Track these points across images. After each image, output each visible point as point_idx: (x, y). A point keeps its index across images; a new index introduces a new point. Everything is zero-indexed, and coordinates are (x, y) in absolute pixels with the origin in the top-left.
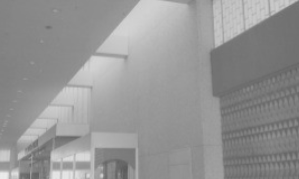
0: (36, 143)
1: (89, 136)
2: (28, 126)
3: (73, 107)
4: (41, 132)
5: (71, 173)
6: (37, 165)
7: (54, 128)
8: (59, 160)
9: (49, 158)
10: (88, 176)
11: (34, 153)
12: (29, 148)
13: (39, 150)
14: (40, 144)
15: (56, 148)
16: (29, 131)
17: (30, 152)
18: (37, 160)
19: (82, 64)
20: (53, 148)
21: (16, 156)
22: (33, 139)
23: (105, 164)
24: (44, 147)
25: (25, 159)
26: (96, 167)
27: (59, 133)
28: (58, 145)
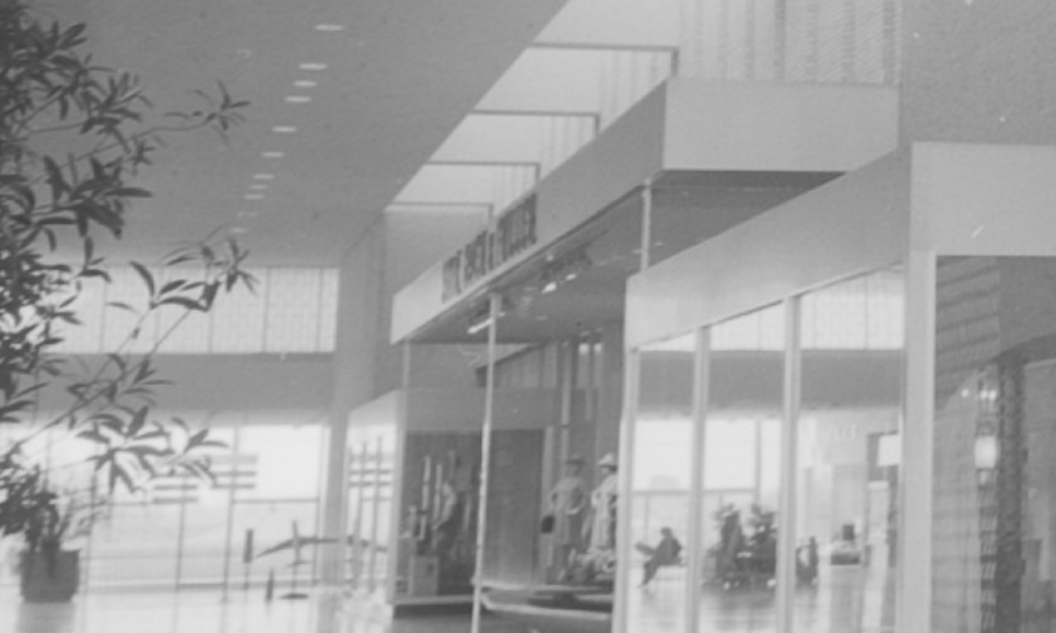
0: (521, 218)
1: (894, 169)
2: (464, 102)
3: (675, 54)
4: (559, 142)
5: (773, 428)
6: (527, 377)
7: (649, 113)
8: (686, 343)
9: (612, 326)
10: (890, 452)
11: (506, 290)
12: (476, 254)
13: (548, 271)
14: (551, 230)
15: (657, 256)
16: (472, 132)
17: (476, 287)
18: (530, 338)
19: (499, 70)
20: (644, 252)
21: (383, 317)
22: (507, 190)
23: (1010, 366)
24: (574, 252)
25: (445, 333)
26: (944, 392)
27: (683, 152)
28: (673, 241)
